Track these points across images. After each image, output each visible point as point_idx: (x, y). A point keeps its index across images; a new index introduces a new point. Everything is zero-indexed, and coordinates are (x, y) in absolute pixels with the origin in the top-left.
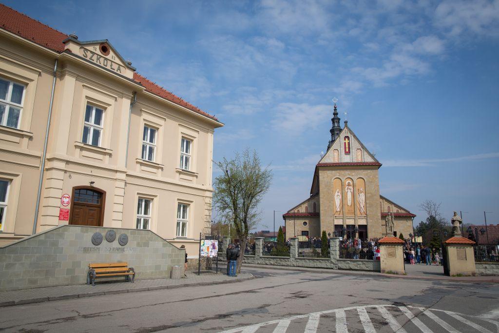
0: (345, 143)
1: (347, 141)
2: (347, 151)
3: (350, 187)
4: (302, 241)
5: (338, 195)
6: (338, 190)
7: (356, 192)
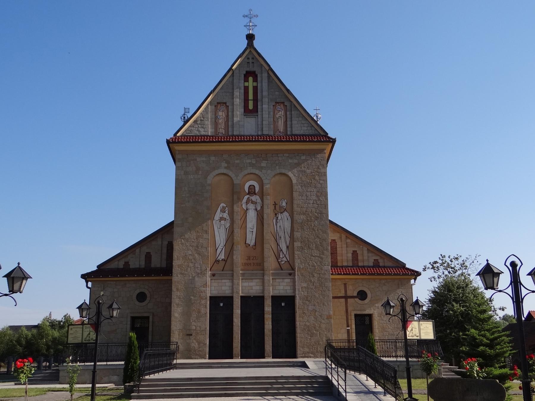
0: (246, 89)
1: (251, 83)
2: (251, 107)
3: (254, 198)
4: (79, 340)
5: (221, 219)
6: (222, 205)
7: (269, 211)
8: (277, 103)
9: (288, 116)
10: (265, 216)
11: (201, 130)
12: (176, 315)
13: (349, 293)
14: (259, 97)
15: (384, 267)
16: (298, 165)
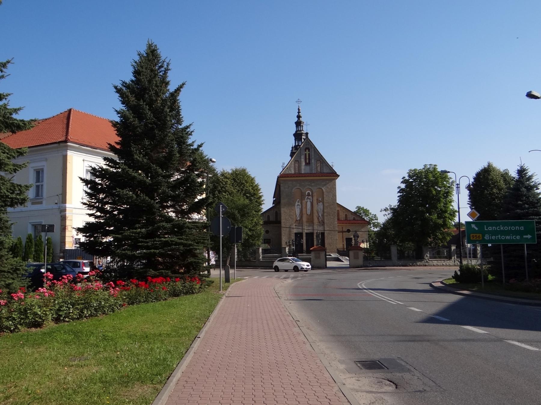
0: (306, 154)
1: (307, 152)
2: (307, 162)
3: (309, 197)
5: (298, 205)
7: (315, 202)
8: (317, 160)
9: (322, 165)
10: (314, 204)
11: (290, 171)
12: (283, 239)
13: (344, 230)
14: (311, 158)
15: (357, 220)
16: (325, 185)
